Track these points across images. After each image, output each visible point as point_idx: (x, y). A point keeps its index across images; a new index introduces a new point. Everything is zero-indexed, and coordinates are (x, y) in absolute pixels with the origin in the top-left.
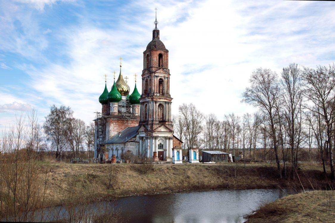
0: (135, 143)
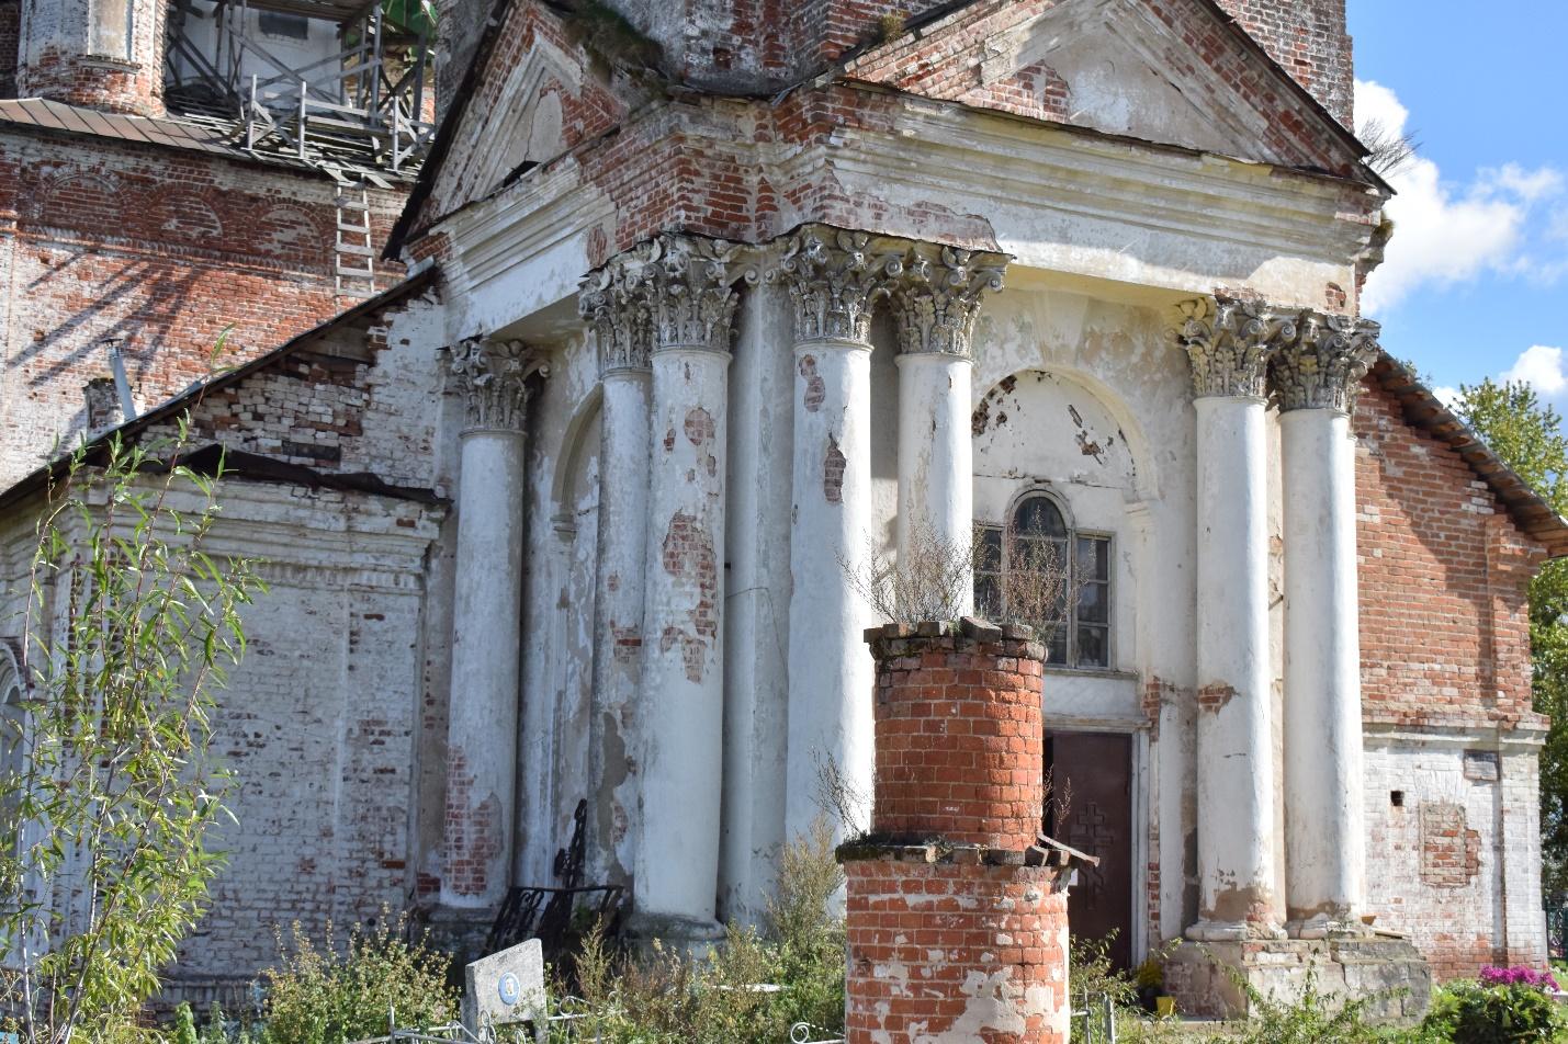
0: (324, 511)
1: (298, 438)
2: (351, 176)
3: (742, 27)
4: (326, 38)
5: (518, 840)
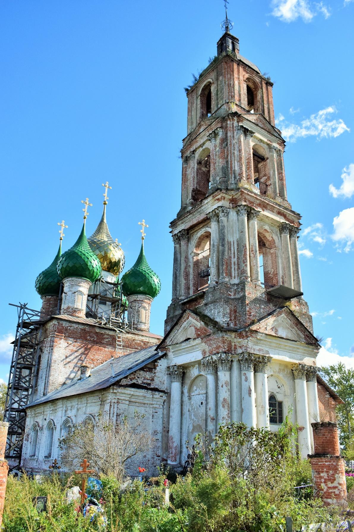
0: (149, 394)
1: (144, 381)
2: (119, 331)
3: (231, 320)
4: (109, 305)
5: (181, 452)
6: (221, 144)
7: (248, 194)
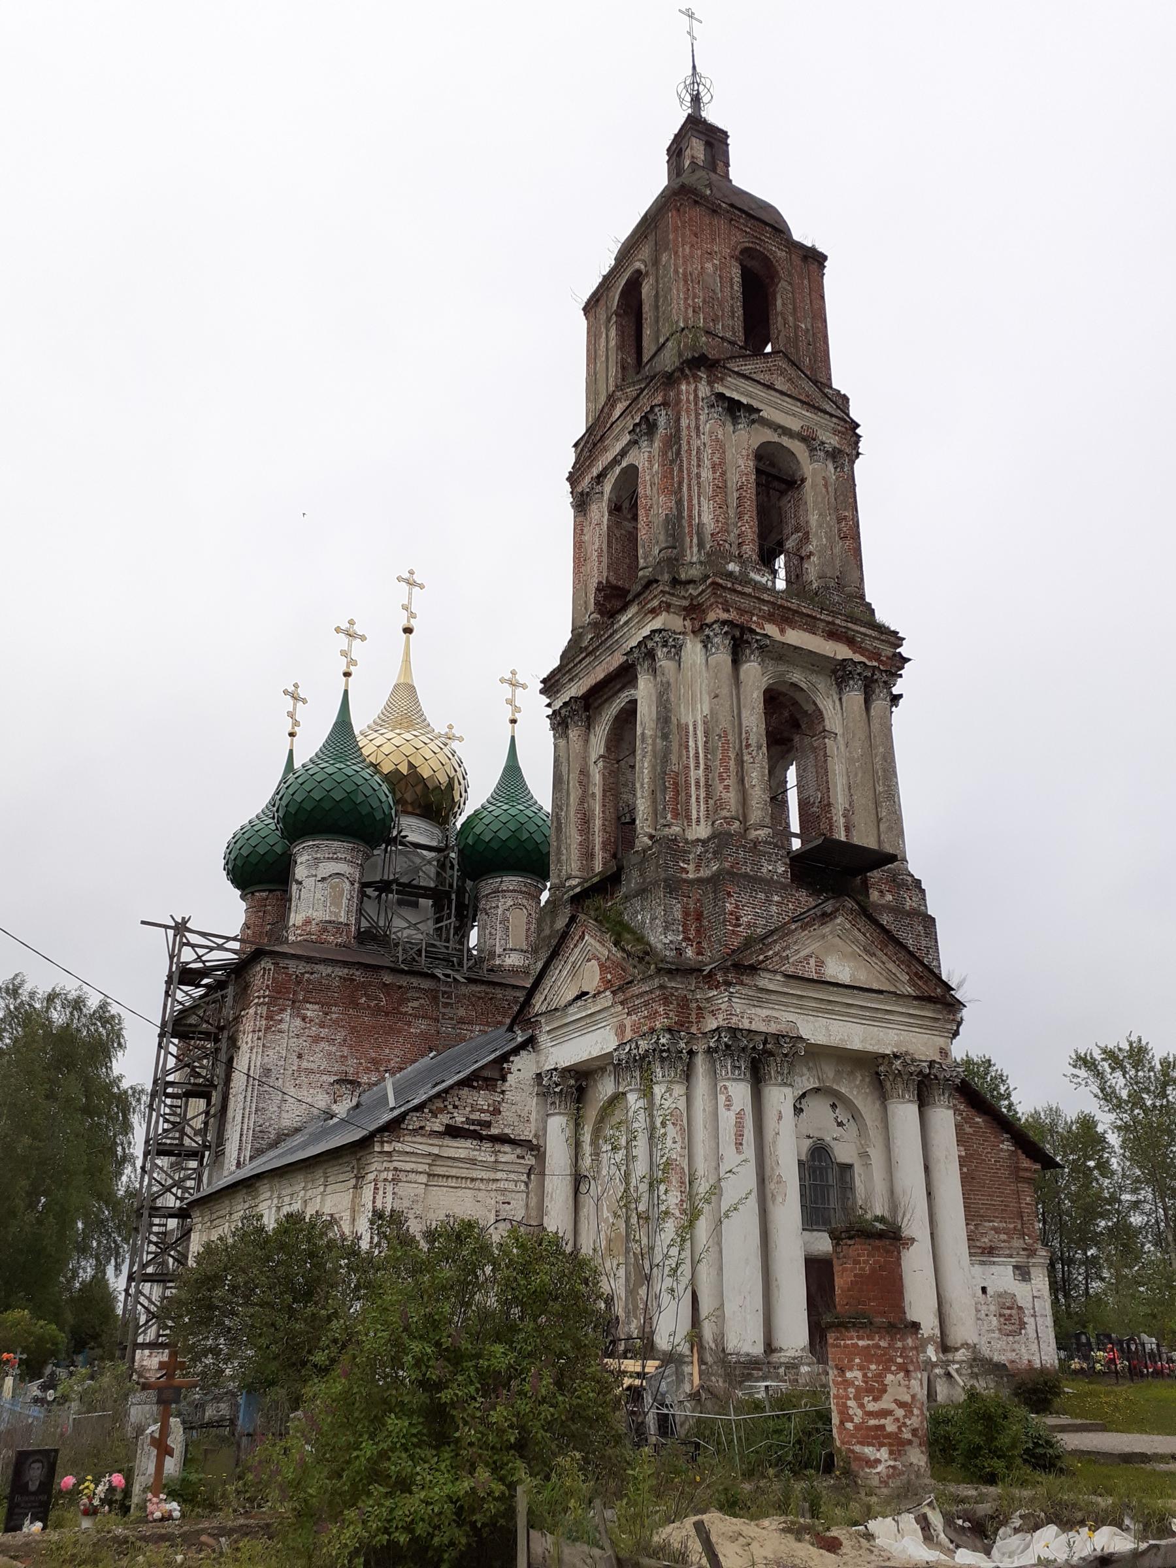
0: (484, 1153)
1: (472, 1117)
6: (664, 453)
7: (735, 591)
